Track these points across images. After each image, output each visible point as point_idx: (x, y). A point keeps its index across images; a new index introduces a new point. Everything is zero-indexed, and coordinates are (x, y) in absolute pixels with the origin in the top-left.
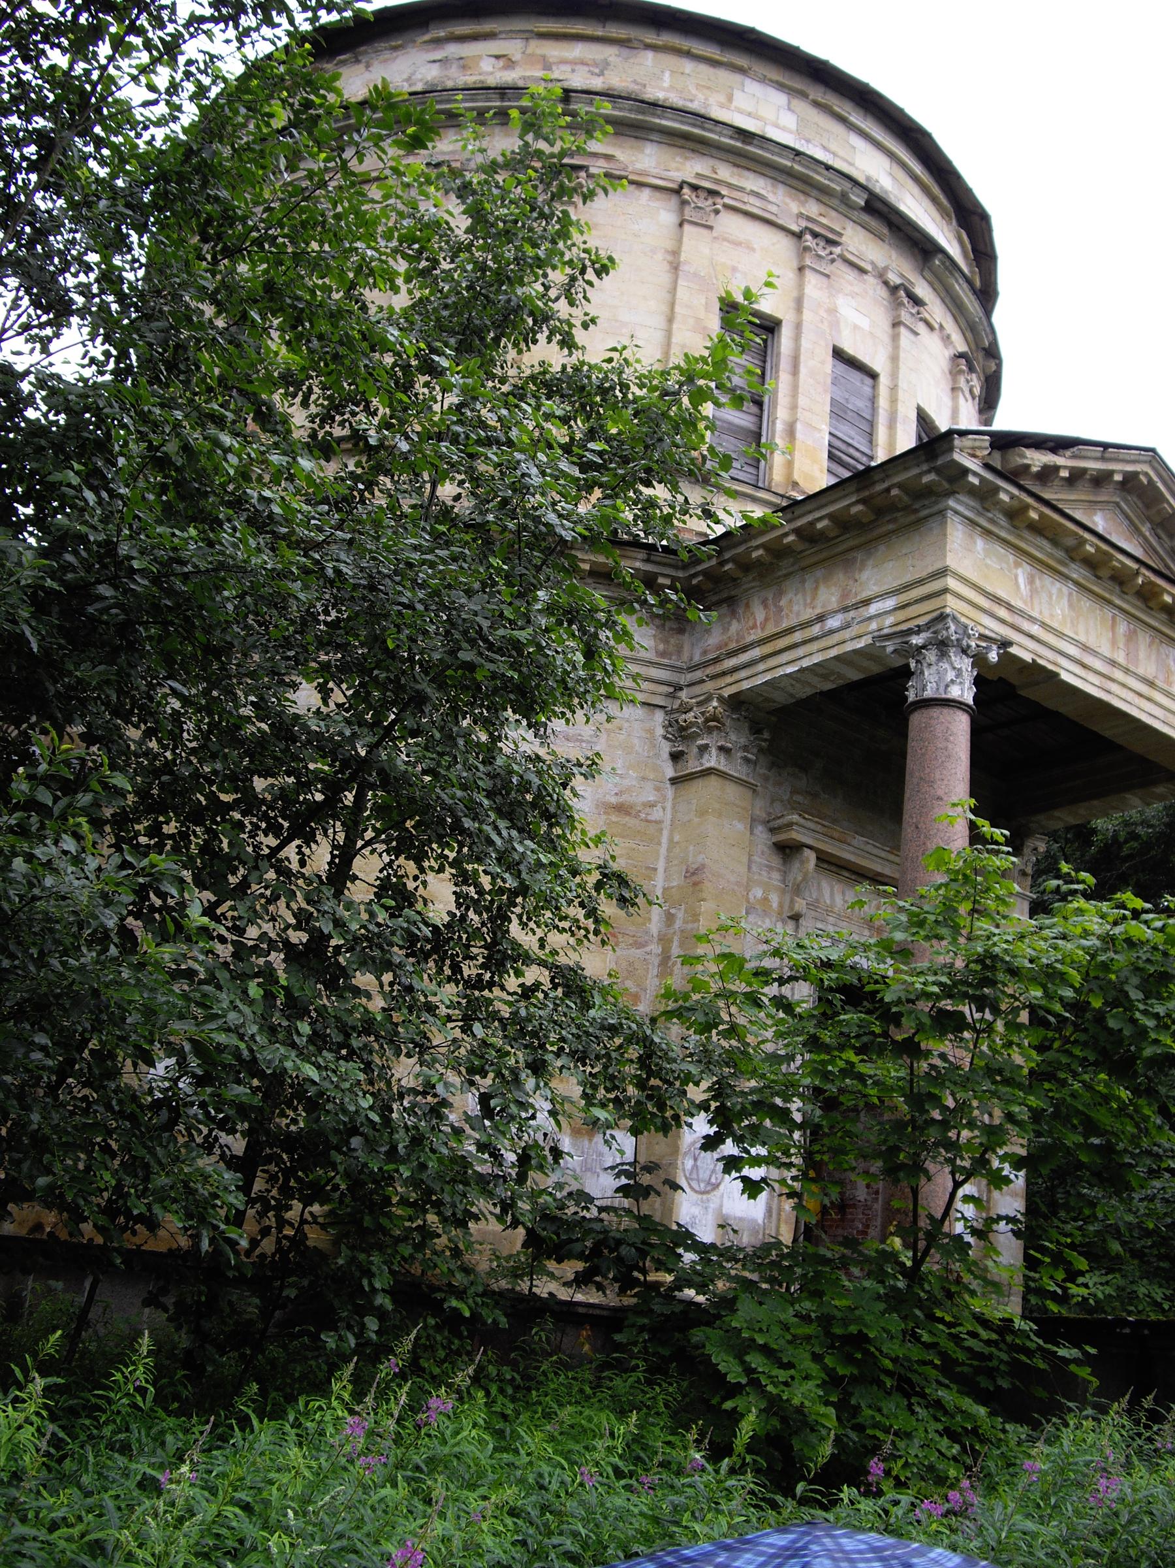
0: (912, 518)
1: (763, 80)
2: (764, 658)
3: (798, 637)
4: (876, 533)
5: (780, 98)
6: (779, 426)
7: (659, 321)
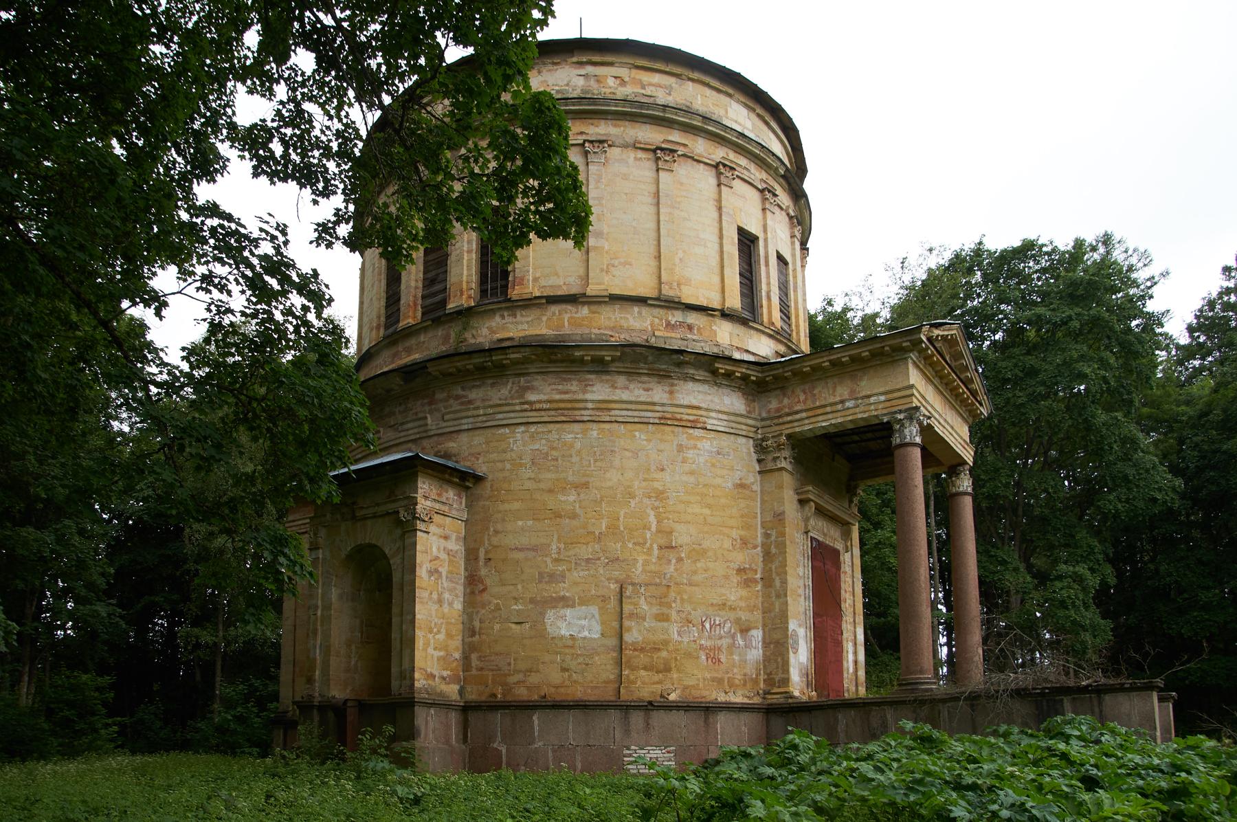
1: (738, 101)
2: (808, 418)
3: (828, 409)
5: (744, 111)
6: (764, 294)
7: (715, 239)
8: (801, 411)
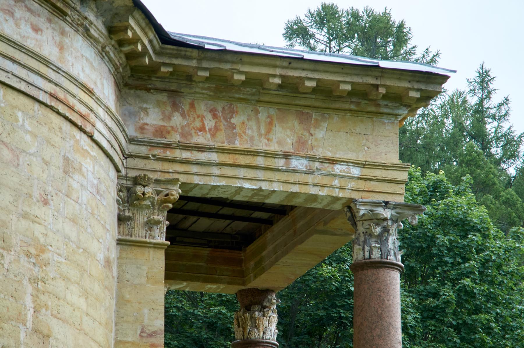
0: (373, 109)
3: (260, 161)
4: (337, 105)
8: (202, 149)
